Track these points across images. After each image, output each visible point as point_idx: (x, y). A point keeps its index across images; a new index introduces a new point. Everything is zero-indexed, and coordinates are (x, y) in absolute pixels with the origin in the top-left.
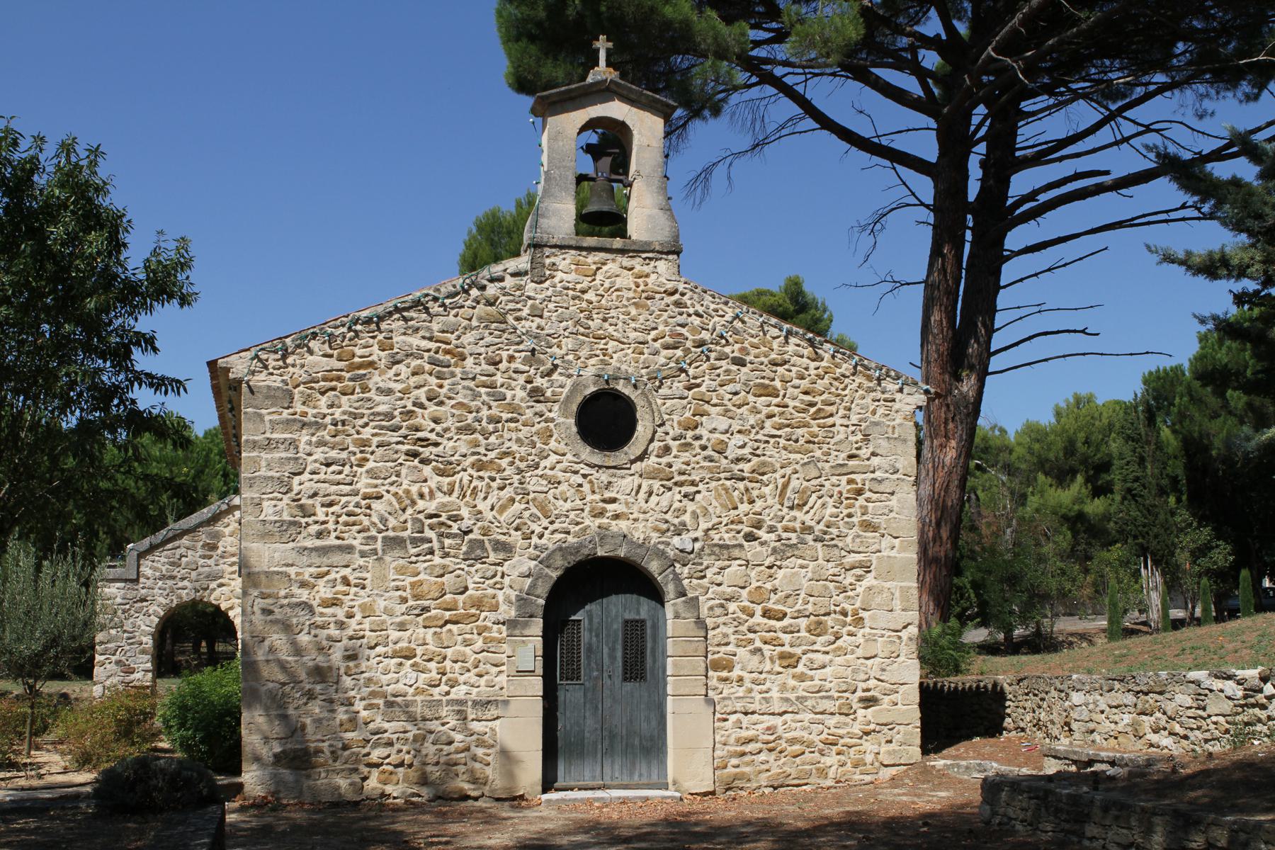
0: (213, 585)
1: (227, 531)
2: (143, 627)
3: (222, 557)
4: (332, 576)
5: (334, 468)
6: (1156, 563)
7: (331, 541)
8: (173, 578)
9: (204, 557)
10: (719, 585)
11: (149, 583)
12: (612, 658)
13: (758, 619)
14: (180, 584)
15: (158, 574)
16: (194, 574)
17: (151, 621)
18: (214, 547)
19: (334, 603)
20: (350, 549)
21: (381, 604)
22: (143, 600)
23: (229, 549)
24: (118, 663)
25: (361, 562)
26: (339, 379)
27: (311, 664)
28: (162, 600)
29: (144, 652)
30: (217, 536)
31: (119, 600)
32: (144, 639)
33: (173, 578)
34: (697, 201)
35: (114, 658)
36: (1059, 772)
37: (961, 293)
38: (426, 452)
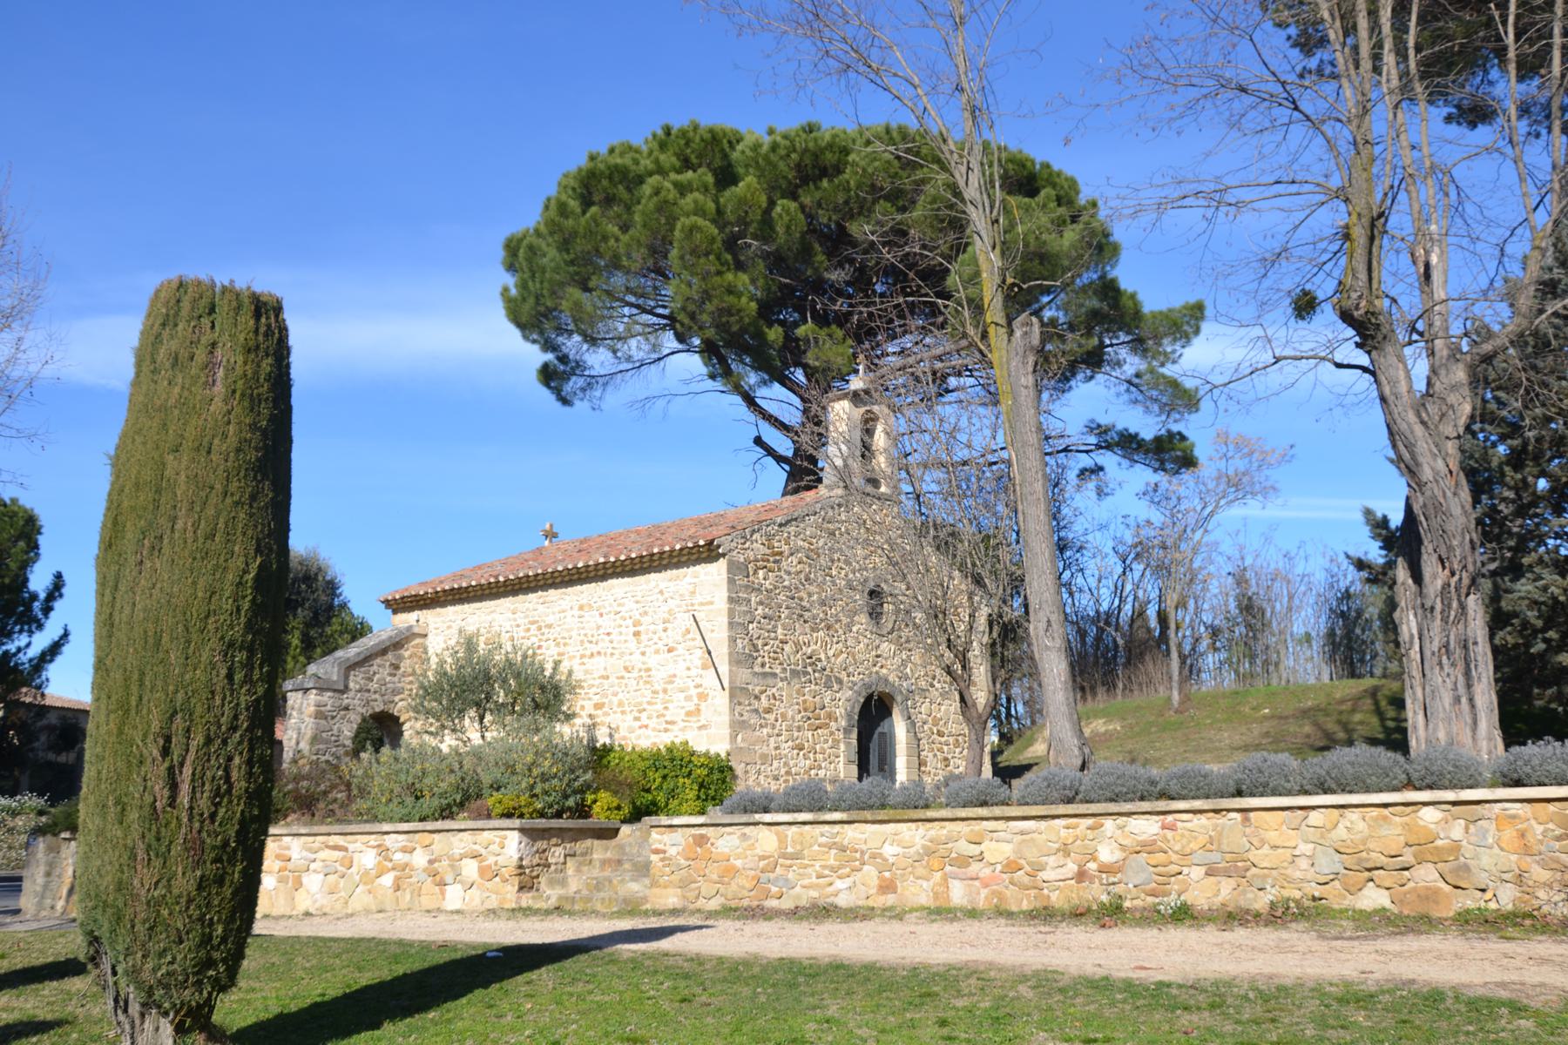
1: (407, 654)
7: (767, 669)
18: (397, 667)
19: (768, 711)
20: (774, 675)
30: (401, 658)
38: (807, 615)
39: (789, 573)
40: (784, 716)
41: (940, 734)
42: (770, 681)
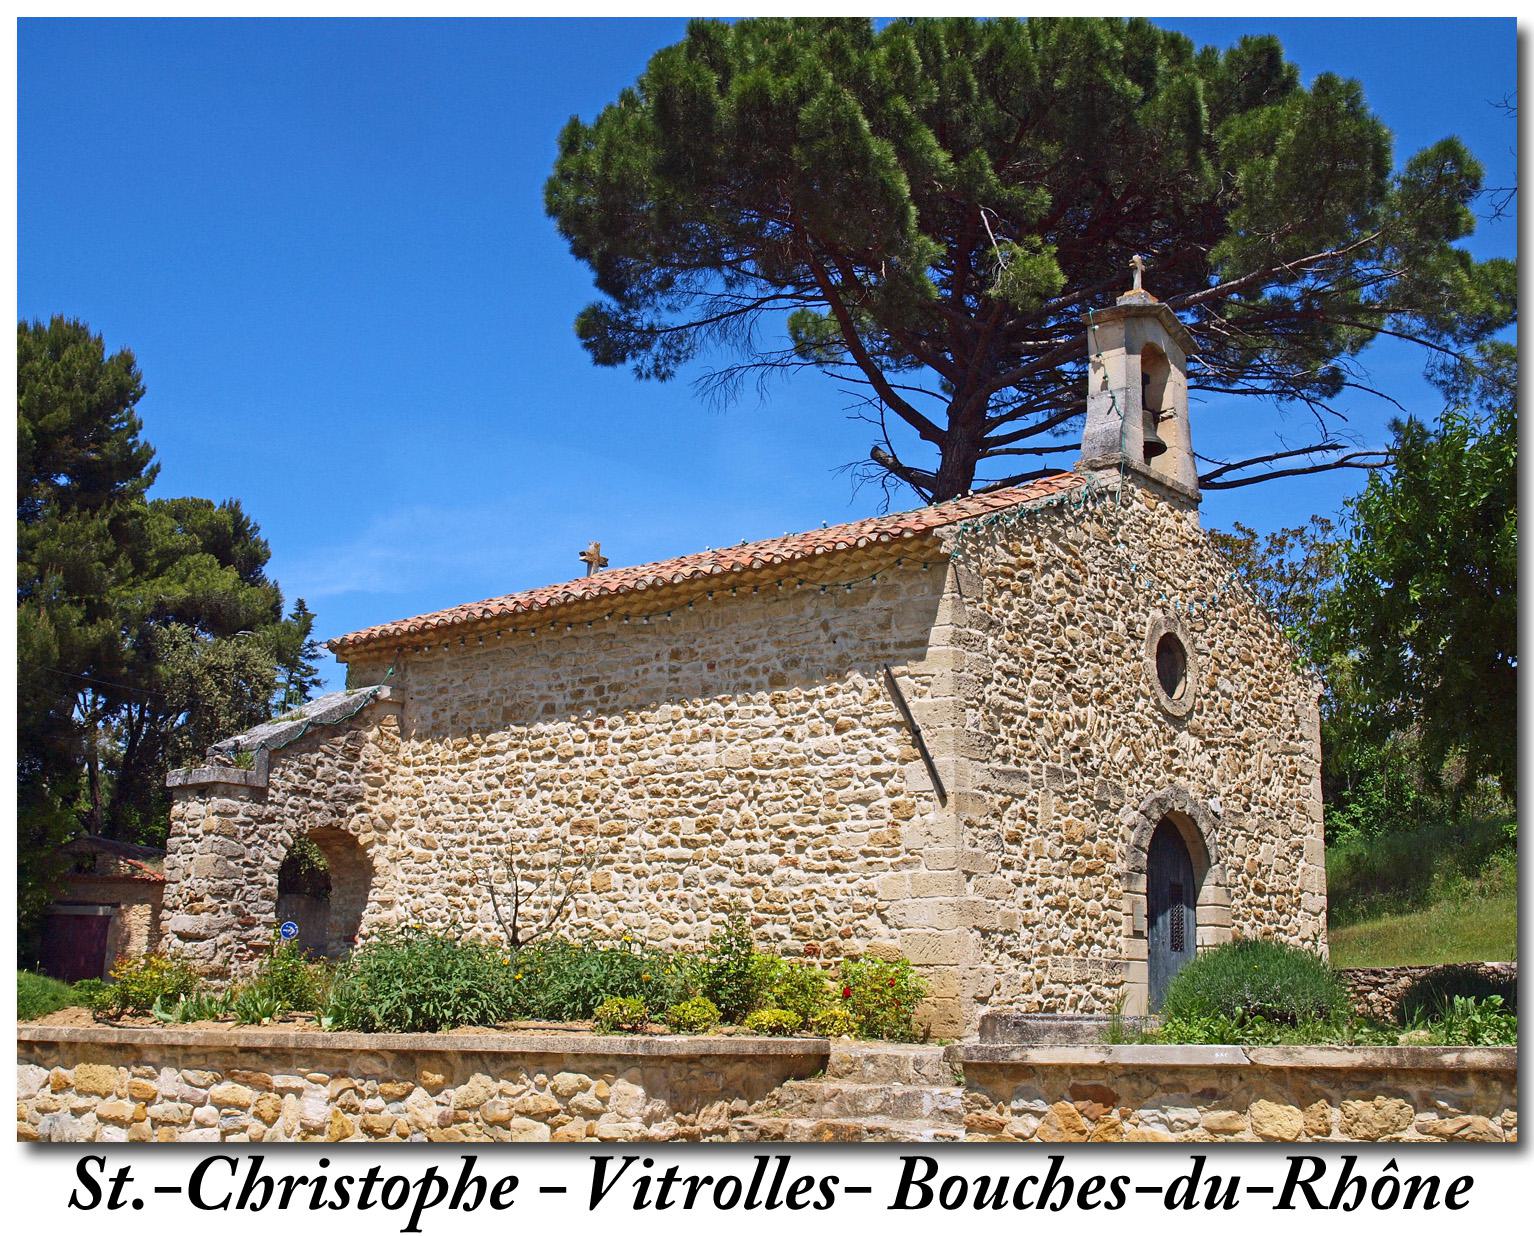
0: (351, 809)
2: (267, 860)
3: (363, 771)
4: (1013, 806)
5: (1012, 680)
6: (1454, 226)
8: (306, 792)
9: (342, 767)
10: (758, 713)
11: (278, 797)
12: (1165, 928)
13: (1251, 894)
14: (314, 803)
15: (289, 784)
16: (330, 791)
17: (279, 853)
18: (356, 757)
19: (1015, 840)
20: (1023, 776)
21: (1047, 844)
22: (270, 819)
23: (371, 760)
24: (237, 910)
25: (1032, 793)
26: (1011, 576)
27: (1190, 515)
28: (291, 823)
29: (266, 897)
31: (240, 817)
32: (269, 878)
33: (306, 792)
34: (722, 405)
35: (229, 904)
36: (1388, 169)
37: (1223, 1055)
39: (1042, 600)
40: (1038, 846)
41: (1259, 891)
42: (1016, 786)
